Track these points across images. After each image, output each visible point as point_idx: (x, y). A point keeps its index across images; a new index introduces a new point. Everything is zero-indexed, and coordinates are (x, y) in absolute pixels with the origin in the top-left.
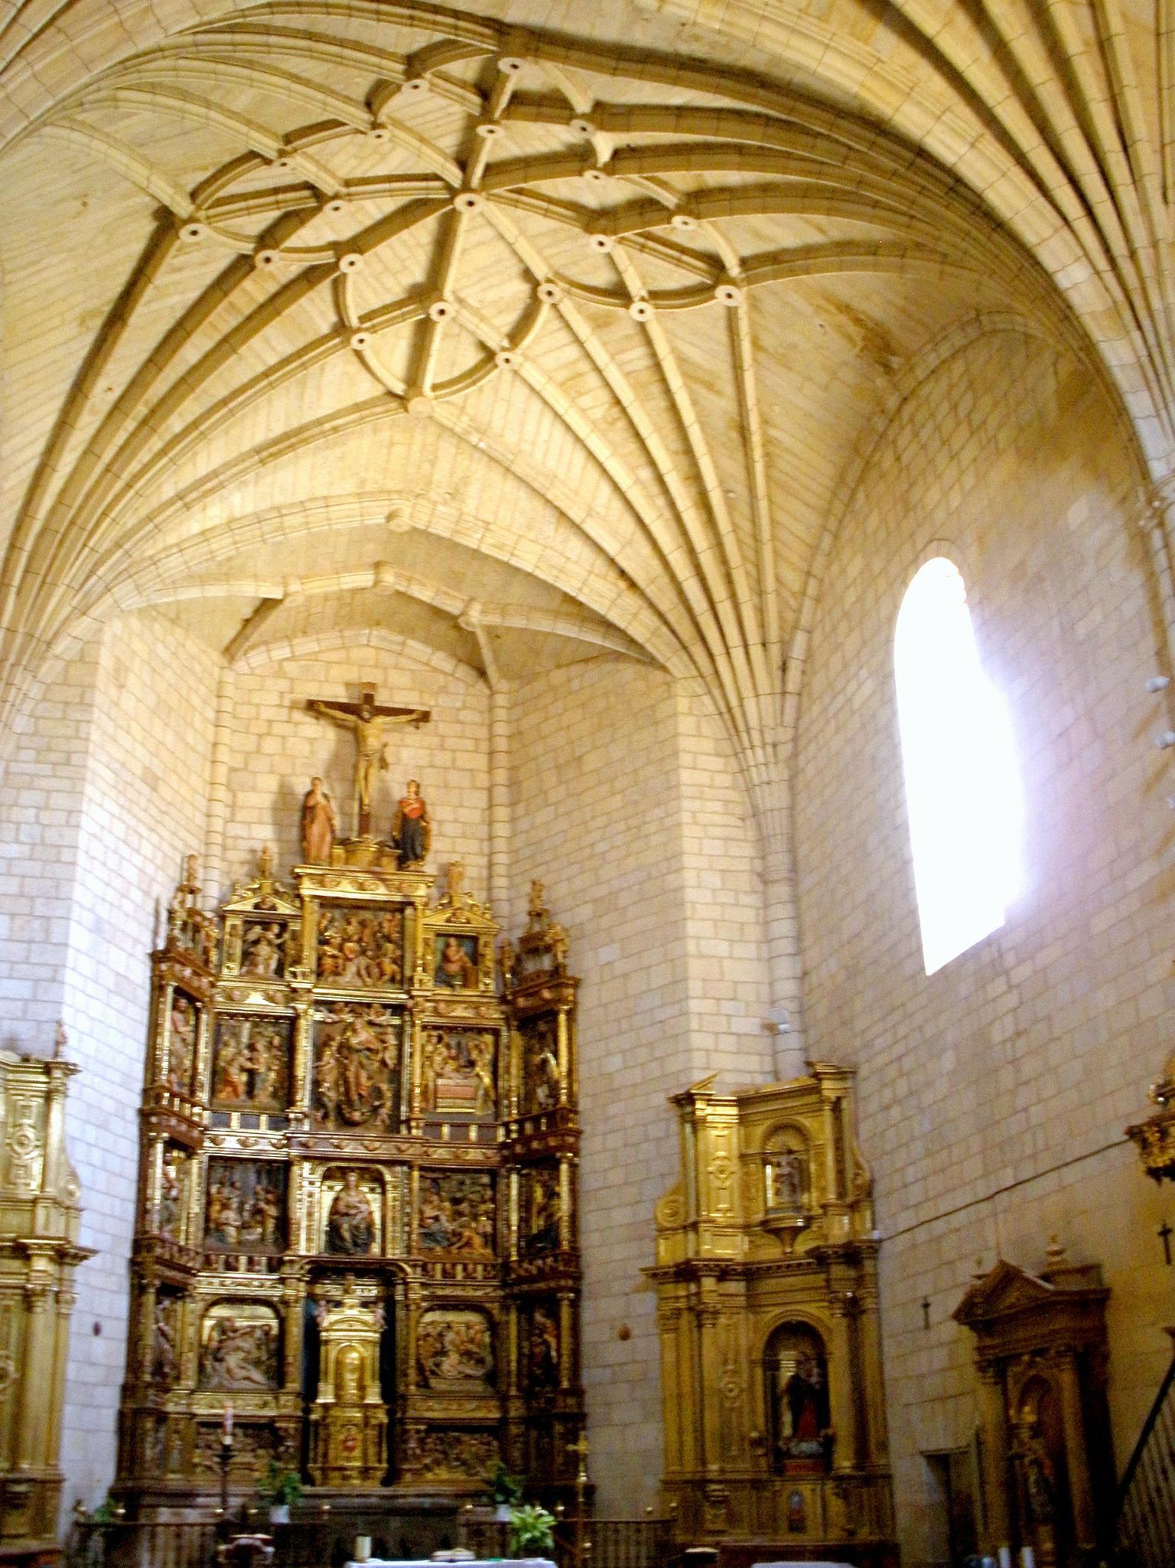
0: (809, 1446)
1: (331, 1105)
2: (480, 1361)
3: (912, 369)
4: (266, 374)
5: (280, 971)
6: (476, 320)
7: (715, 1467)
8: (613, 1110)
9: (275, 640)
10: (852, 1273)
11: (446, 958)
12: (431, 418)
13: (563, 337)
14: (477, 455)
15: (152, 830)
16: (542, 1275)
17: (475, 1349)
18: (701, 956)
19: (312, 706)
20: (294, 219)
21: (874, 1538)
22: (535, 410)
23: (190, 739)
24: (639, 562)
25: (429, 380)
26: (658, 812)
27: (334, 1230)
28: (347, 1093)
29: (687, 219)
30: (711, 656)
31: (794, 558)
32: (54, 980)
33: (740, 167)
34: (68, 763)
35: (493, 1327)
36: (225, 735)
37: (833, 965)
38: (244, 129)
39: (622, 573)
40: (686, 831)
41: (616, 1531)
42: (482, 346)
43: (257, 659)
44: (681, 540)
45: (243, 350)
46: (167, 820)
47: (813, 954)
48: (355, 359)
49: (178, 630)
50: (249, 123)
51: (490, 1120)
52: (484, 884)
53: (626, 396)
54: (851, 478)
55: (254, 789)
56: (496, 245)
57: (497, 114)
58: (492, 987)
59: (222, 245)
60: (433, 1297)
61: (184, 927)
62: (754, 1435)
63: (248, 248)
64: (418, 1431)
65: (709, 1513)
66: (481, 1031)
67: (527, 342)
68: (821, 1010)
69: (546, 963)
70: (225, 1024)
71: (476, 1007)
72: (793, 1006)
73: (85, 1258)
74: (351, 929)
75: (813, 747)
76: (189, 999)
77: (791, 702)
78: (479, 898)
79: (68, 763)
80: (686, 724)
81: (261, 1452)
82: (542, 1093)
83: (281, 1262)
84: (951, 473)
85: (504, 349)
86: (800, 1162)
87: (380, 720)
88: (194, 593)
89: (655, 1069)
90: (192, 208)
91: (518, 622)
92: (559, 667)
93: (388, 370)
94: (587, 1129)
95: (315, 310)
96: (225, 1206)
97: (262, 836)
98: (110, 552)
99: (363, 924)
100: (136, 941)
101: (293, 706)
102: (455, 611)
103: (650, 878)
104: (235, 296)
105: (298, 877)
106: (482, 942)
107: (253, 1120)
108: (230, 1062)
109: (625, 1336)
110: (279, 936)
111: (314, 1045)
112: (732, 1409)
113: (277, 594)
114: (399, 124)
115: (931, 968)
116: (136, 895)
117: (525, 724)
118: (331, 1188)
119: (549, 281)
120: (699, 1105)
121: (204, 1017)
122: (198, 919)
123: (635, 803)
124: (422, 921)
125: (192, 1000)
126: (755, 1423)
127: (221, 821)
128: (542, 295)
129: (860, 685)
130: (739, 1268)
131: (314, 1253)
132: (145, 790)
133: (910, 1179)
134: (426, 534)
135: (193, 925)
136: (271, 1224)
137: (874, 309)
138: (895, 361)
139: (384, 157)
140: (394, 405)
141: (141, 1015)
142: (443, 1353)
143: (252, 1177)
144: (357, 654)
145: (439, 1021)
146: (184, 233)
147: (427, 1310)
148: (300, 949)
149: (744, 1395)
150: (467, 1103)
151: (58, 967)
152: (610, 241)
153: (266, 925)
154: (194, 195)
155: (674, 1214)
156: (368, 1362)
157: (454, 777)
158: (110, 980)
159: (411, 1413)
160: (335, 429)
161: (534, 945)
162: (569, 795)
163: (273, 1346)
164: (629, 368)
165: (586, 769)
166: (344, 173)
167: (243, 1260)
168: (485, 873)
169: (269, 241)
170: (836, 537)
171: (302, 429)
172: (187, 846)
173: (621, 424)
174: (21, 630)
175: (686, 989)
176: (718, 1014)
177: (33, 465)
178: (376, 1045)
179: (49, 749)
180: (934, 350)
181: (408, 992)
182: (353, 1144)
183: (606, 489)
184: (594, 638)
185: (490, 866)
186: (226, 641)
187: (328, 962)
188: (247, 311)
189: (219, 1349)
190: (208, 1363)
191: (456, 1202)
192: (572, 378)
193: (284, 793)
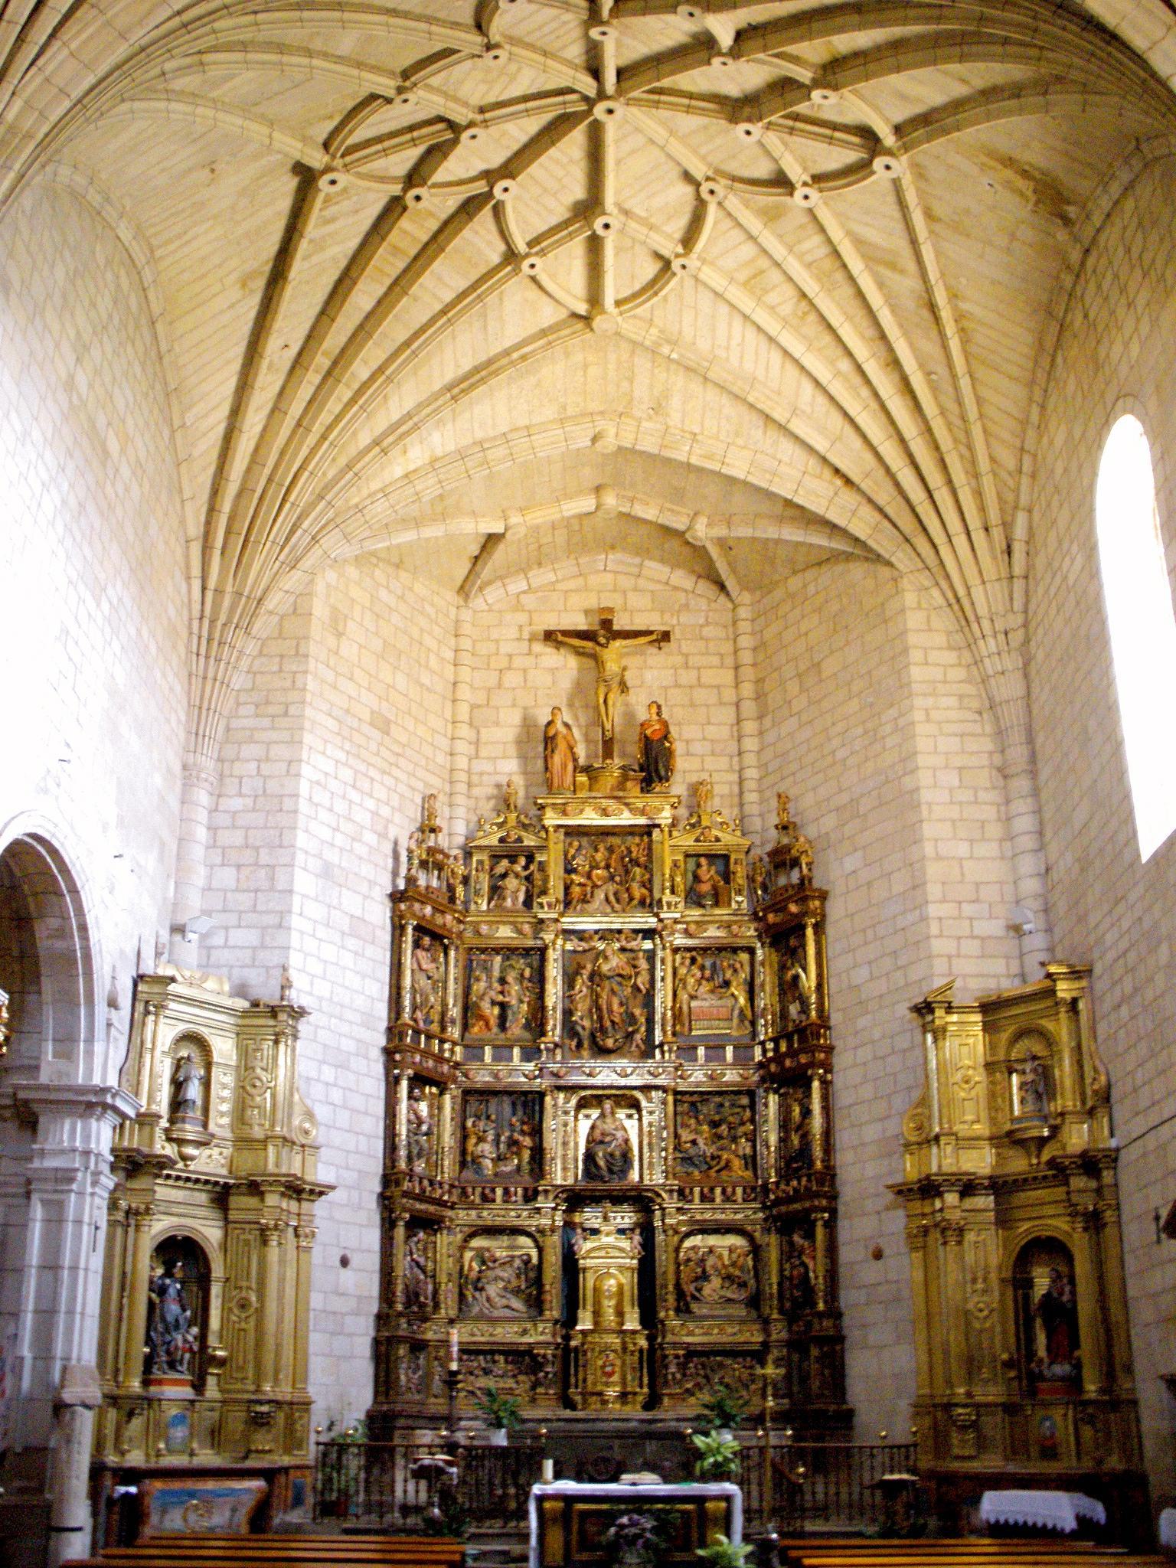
0: (1061, 1369)
1: (585, 1034)
2: (743, 1285)
3: (1088, 217)
4: (443, 312)
5: (528, 903)
6: (645, 230)
7: (962, 1390)
8: (862, 1022)
9: (508, 575)
10: (1093, 1184)
11: (697, 879)
12: (618, 334)
13: (737, 235)
14: (673, 366)
15: (384, 772)
16: (797, 1197)
17: (737, 1273)
18: (939, 858)
19: (549, 636)
20: (436, 153)
21: (1121, 1467)
22: (736, 311)
23: (426, 679)
24: (852, 458)
25: (609, 300)
26: (893, 712)
27: (590, 1157)
28: (600, 1018)
29: (826, 92)
30: (934, 546)
31: (1005, 435)
32: (280, 926)
33: (860, 27)
34: (286, 714)
35: (756, 1250)
36: (465, 673)
37: (1069, 857)
38: (355, 72)
39: (837, 471)
40: (920, 729)
41: (872, 1456)
42: (658, 256)
43: (493, 594)
44: (891, 430)
45: (414, 289)
46: (402, 762)
47: (1053, 848)
48: (533, 286)
49: (403, 574)
50: (359, 65)
51: (746, 1041)
52: (736, 800)
53: (811, 287)
54: (1049, 342)
55: (497, 724)
56: (651, 151)
57: (605, 13)
58: (745, 905)
59: (369, 189)
60: (692, 1221)
61: (424, 864)
62: (1005, 1356)
63: (396, 189)
64: (677, 1357)
65: (955, 1438)
66: (735, 950)
67: (699, 246)
68: (1062, 906)
69: (795, 876)
70: (476, 955)
71: (728, 926)
72: (1037, 905)
73: (321, 1193)
74: (599, 856)
75: (1040, 631)
76: (431, 936)
77: (1019, 585)
78: (729, 814)
79: (286, 714)
80: (914, 620)
81: (521, 1378)
82: (794, 1009)
83: (536, 1193)
84: (1129, 325)
85: (677, 256)
86: (1044, 1067)
87: (617, 644)
88: (408, 536)
89: (899, 978)
90: (326, 158)
91: (743, 531)
92: (794, 573)
93: (569, 292)
94: (838, 1044)
95: (479, 241)
96: (481, 1140)
97: (506, 770)
98: (312, 505)
99: (611, 850)
100: (372, 883)
101: (532, 639)
102: (682, 527)
103: (887, 782)
104: (394, 237)
105: (542, 807)
106: (733, 857)
107: (505, 1052)
108: (481, 997)
109: (878, 1255)
110: (526, 868)
111: (565, 973)
112: (981, 1331)
113: (498, 528)
114: (513, 41)
115: (1146, 854)
116: (370, 838)
117: (768, 634)
118: (587, 1116)
119: (708, 179)
120: (939, 1013)
121: (452, 953)
122: (440, 857)
123: (871, 705)
124: (668, 843)
125: (437, 937)
126: (1000, 1344)
127: (465, 760)
128: (705, 195)
129: (1073, 560)
130: (986, 1182)
131: (570, 1181)
132: (376, 734)
133: (1139, 1082)
134: (633, 451)
135: (433, 861)
136: (526, 1155)
137: (1035, 156)
138: (1072, 211)
139: (513, 78)
140: (580, 325)
141: (383, 956)
142: (705, 1277)
143: (507, 1108)
144: (594, 580)
145: (690, 942)
146: (323, 182)
147: (688, 1235)
148: (546, 880)
149: (995, 1315)
150: (722, 1024)
151: (284, 914)
152: (756, 128)
153: (513, 859)
154: (326, 145)
155: (919, 1128)
156: (627, 1288)
157: (700, 695)
158: (345, 924)
159: (669, 1338)
160: (524, 358)
161: (782, 859)
162: (810, 703)
163: (532, 1275)
164: (809, 258)
165: (824, 676)
166: (476, 100)
167: (499, 1192)
168: (736, 789)
169: (416, 179)
170: (1043, 407)
171: (490, 362)
172: (427, 784)
173: (812, 317)
174: (229, 589)
175: (925, 893)
176: (960, 917)
177: (221, 429)
178: (628, 971)
179: (267, 703)
180: (1105, 191)
181: (656, 915)
182: (606, 1072)
183: (808, 387)
184: (819, 539)
185: (741, 781)
186: (459, 582)
187: (576, 890)
188: (413, 252)
189: (479, 1279)
190: (469, 1294)
191: (715, 1124)
192: (754, 277)
193: (528, 724)
